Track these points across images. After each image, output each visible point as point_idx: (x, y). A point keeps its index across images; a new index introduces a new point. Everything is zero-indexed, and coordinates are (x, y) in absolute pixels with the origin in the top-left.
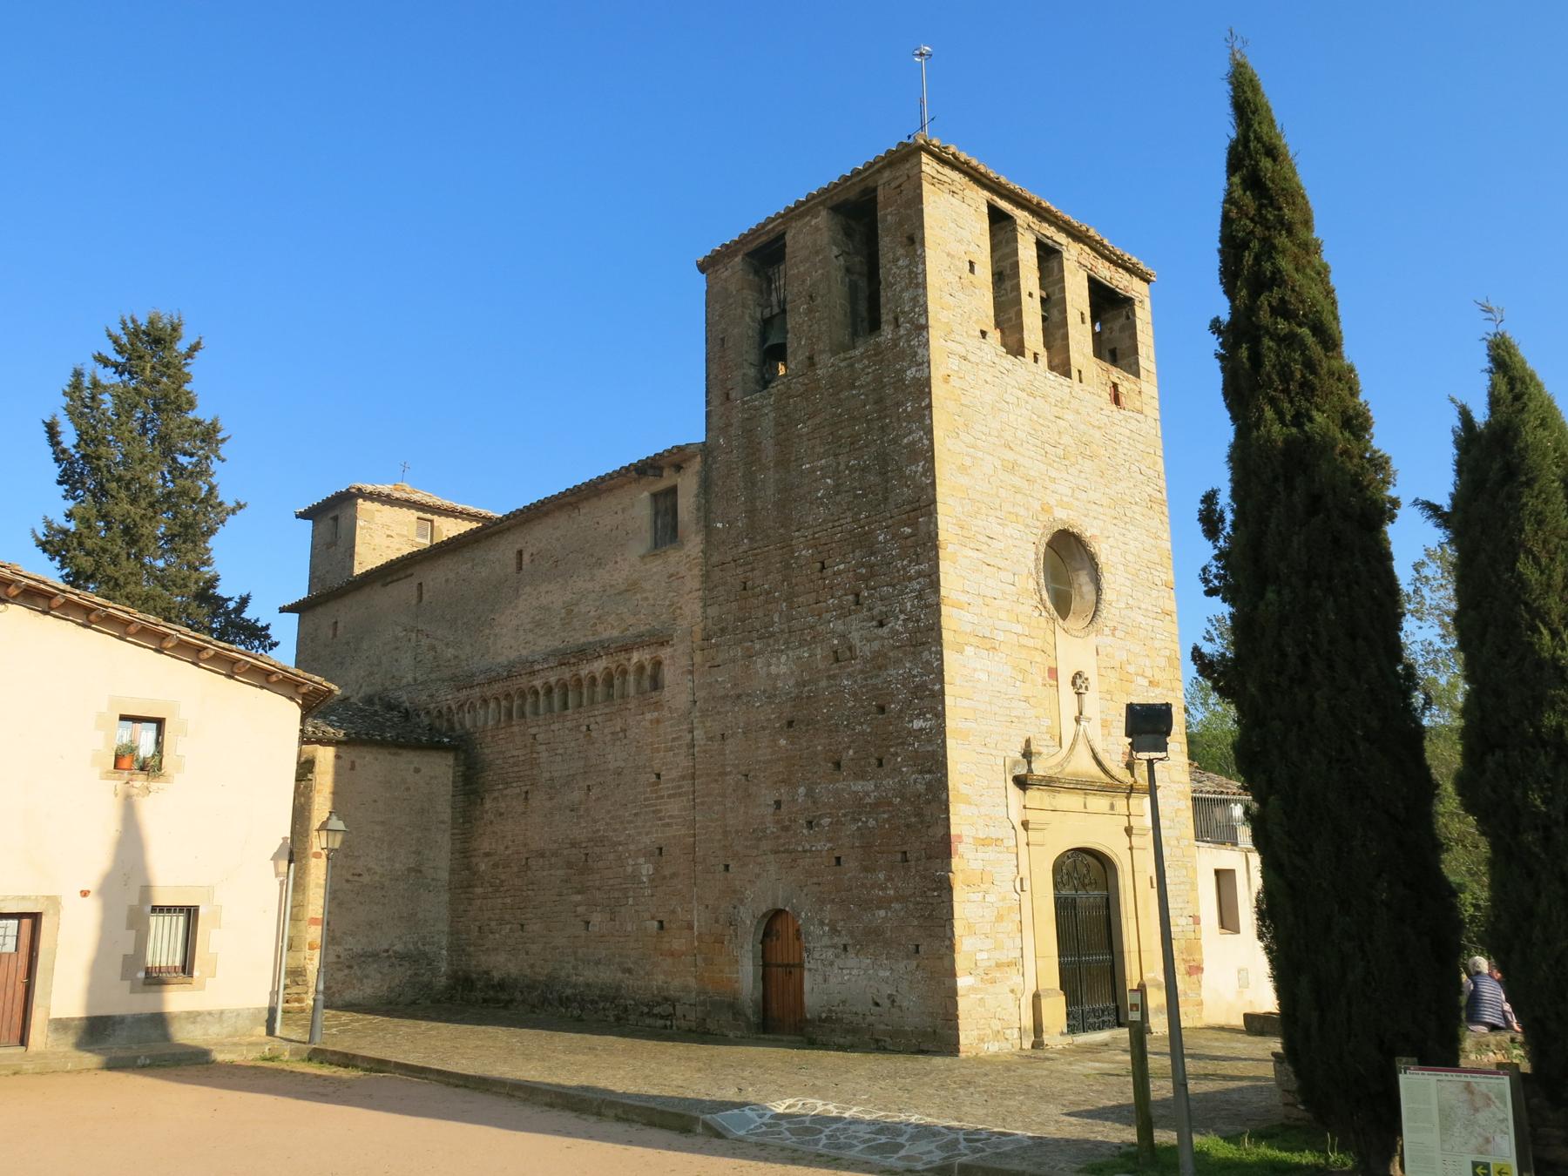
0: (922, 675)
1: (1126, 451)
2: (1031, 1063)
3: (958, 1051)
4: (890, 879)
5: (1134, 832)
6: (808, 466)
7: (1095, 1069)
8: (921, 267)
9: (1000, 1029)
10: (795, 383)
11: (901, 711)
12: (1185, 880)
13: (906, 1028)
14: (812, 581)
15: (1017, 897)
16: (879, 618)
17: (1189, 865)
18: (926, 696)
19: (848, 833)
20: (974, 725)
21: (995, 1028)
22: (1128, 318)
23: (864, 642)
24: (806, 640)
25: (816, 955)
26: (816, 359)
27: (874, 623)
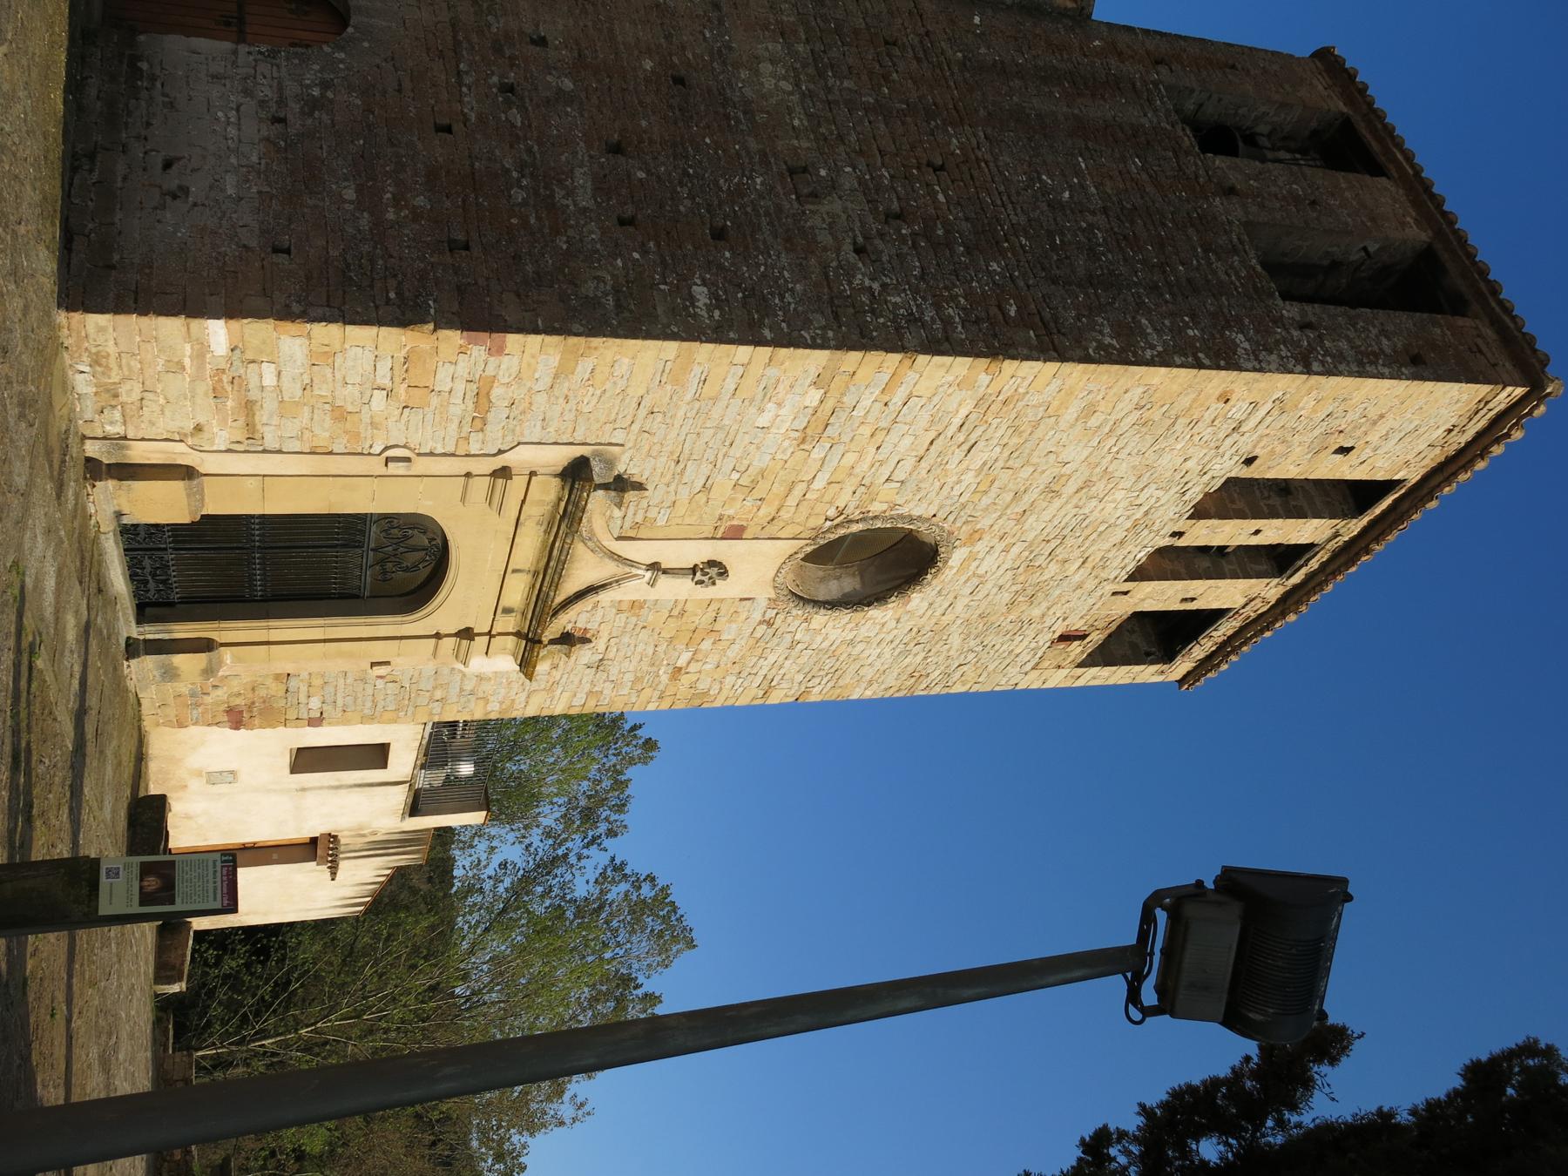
0: (785, 309)
1: (996, 648)
2: (49, 453)
3: (71, 308)
4: (416, 215)
5: (465, 643)
6: (1083, 165)
7: (38, 581)
8: (1386, 371)
9: (123, 398)
10: (1196, 165)
11: (721, 267)
12: (379, 707)
13: (119, 216)
14: (913, 148)
15: (377, 449)
16: (869, 248)
17: (402, 714)
18: (749, 313)
19: (497, 152)
20: (689, 397)
21: (123, 390)
22: (1148, 654)
23: (828, 220)
24: (819, 125)
25: (264, 68)
26: (1235, 199)
27: (860, 239)
